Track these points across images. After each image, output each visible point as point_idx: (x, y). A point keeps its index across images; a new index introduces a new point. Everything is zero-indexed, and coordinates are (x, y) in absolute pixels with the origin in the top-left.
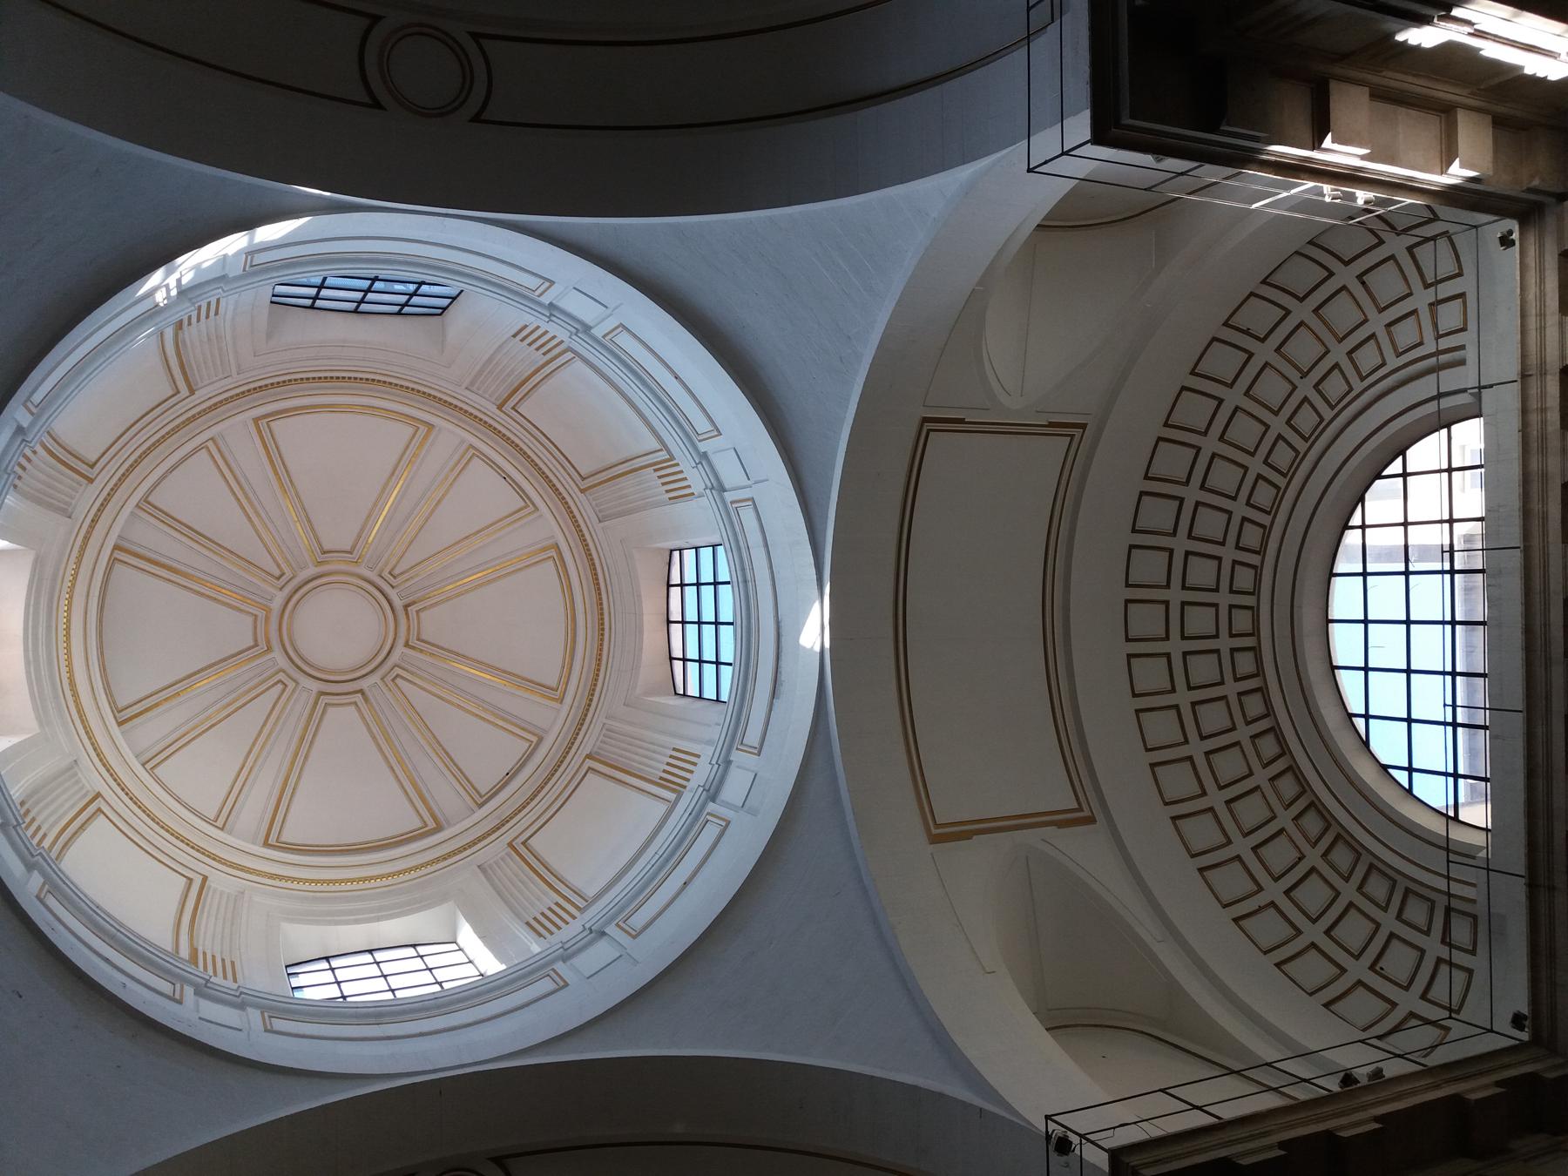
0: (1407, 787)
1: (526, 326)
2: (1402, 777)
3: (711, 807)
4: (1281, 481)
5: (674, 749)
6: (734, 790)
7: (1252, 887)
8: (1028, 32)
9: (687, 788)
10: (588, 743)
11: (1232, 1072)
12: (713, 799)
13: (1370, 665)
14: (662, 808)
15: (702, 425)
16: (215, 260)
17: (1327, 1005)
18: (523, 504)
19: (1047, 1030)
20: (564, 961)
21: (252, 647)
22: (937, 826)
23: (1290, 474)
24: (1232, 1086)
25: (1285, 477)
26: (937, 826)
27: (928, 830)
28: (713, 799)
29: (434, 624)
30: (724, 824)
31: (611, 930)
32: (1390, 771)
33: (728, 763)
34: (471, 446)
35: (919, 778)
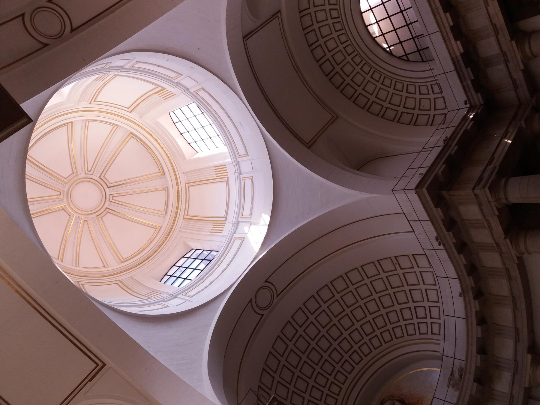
0: (407, 59)
1: (165, 99)
2: (405, 58)
3: (242, 176)
4: (339, 20)
5: (214, 167)
6: (246, 167)
7: (327, 363)
8: (436, 249)
9: (229, 175)
10: (183, 180)
11: (421, 152)
12: (241, 174)
13: (384, 33)
14: (224, 184)
15: (173, 75)
16: (36, 124)
17: (414, 125)
18: (113, 127)
19: (358, 170)
20: (235, 233)
21: (109, 213)
22: (308, 144)
23: (340, 15)
24: (423, 155)
25: (343, 29)
26: (308, 144)
27: (306, 146)
28: (241, 174)
29: (112, 177)
30: (251, 178)
31: (240, 220)
32: (402, 58)
33: (238, 163)
34: (86, 120)
35: (110, 79)
